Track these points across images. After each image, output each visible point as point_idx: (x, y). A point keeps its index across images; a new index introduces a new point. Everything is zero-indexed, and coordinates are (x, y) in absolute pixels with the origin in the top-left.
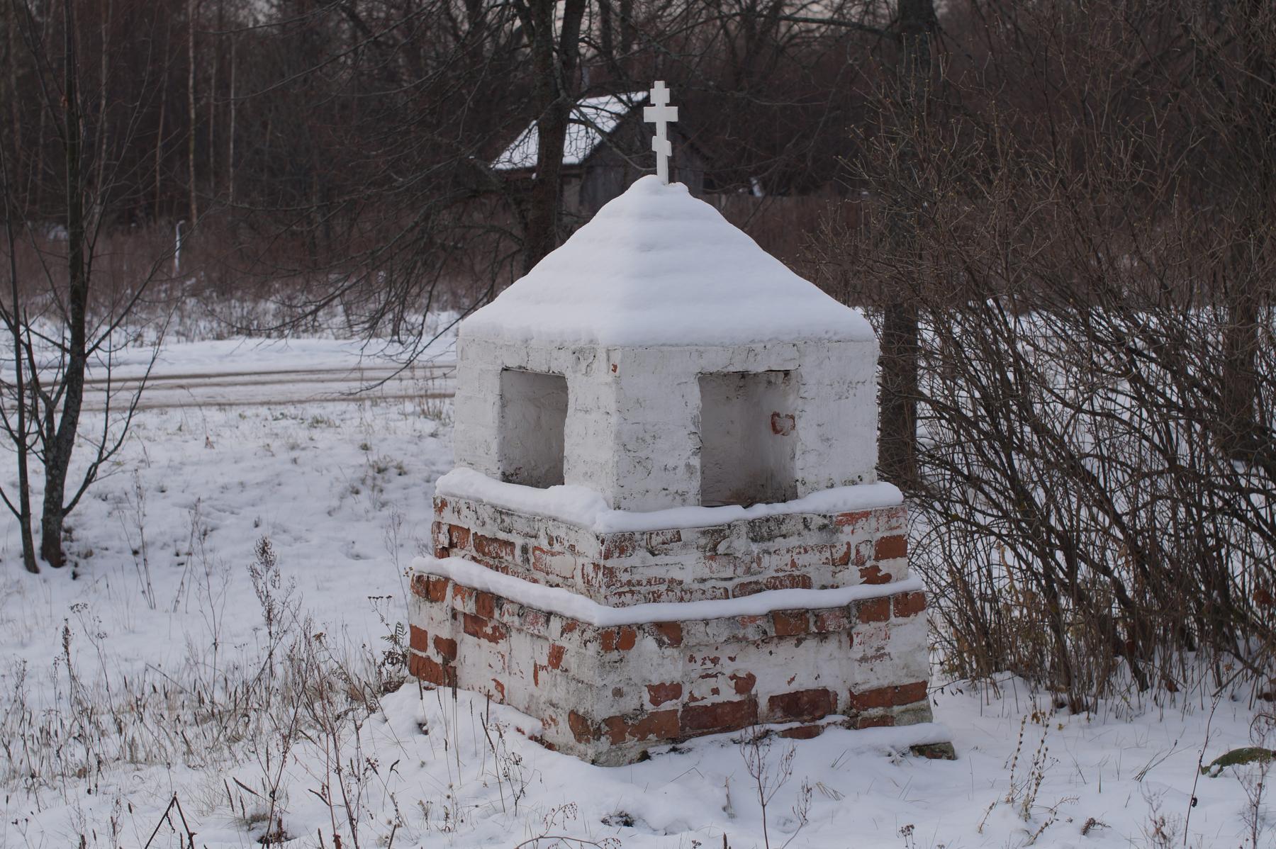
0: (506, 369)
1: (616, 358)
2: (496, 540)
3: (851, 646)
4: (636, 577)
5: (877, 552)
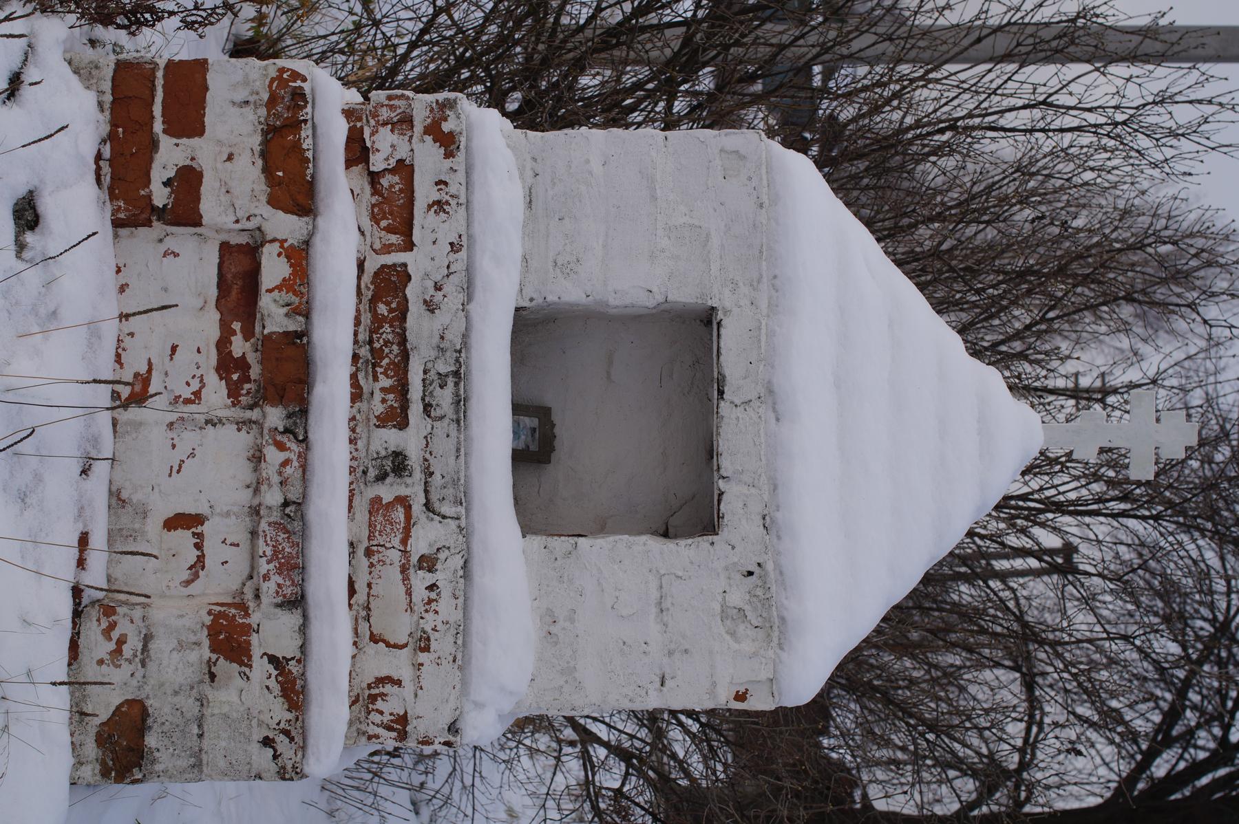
2: (405, 355)
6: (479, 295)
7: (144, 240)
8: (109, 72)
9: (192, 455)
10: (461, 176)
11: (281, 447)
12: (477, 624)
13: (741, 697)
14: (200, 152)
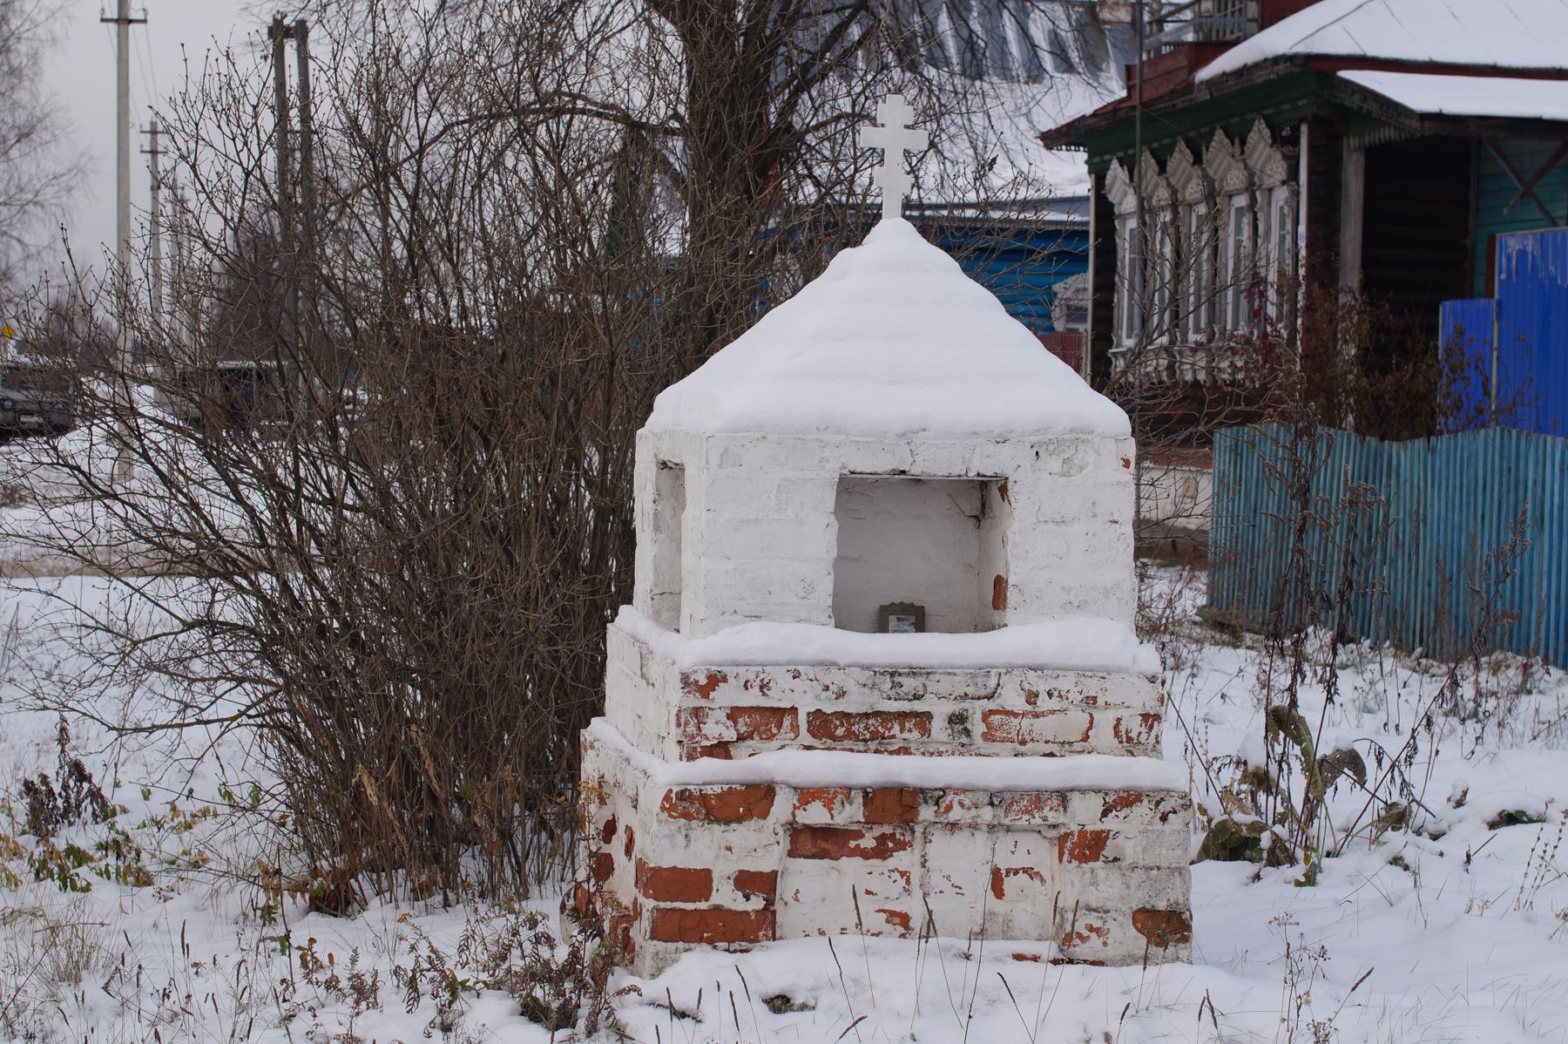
2: (877, 714)
7: (783, 917)
8: (660, 945)
9: (948, 878)
10: (742, 670)
11: (949, 808)
12: (1077, 661)
13: (1127, 464)
14: (723, 871)
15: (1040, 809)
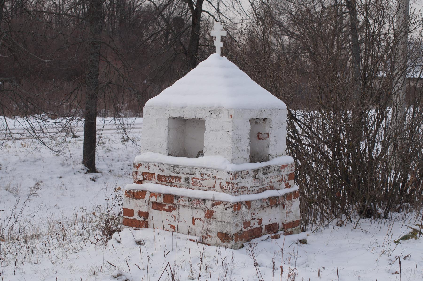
0: (170, 118)
1: (232, 113)
2: (170, 176)
3: (284, 208)
4: (239, 186)
5: (289, 178)
6: (162, 162)
10: (144, 163)
11: (180, 201)
12: (211, 167)
14: (136, 210)
15: (199, 203)
